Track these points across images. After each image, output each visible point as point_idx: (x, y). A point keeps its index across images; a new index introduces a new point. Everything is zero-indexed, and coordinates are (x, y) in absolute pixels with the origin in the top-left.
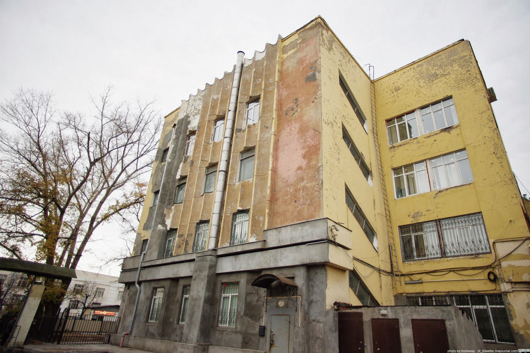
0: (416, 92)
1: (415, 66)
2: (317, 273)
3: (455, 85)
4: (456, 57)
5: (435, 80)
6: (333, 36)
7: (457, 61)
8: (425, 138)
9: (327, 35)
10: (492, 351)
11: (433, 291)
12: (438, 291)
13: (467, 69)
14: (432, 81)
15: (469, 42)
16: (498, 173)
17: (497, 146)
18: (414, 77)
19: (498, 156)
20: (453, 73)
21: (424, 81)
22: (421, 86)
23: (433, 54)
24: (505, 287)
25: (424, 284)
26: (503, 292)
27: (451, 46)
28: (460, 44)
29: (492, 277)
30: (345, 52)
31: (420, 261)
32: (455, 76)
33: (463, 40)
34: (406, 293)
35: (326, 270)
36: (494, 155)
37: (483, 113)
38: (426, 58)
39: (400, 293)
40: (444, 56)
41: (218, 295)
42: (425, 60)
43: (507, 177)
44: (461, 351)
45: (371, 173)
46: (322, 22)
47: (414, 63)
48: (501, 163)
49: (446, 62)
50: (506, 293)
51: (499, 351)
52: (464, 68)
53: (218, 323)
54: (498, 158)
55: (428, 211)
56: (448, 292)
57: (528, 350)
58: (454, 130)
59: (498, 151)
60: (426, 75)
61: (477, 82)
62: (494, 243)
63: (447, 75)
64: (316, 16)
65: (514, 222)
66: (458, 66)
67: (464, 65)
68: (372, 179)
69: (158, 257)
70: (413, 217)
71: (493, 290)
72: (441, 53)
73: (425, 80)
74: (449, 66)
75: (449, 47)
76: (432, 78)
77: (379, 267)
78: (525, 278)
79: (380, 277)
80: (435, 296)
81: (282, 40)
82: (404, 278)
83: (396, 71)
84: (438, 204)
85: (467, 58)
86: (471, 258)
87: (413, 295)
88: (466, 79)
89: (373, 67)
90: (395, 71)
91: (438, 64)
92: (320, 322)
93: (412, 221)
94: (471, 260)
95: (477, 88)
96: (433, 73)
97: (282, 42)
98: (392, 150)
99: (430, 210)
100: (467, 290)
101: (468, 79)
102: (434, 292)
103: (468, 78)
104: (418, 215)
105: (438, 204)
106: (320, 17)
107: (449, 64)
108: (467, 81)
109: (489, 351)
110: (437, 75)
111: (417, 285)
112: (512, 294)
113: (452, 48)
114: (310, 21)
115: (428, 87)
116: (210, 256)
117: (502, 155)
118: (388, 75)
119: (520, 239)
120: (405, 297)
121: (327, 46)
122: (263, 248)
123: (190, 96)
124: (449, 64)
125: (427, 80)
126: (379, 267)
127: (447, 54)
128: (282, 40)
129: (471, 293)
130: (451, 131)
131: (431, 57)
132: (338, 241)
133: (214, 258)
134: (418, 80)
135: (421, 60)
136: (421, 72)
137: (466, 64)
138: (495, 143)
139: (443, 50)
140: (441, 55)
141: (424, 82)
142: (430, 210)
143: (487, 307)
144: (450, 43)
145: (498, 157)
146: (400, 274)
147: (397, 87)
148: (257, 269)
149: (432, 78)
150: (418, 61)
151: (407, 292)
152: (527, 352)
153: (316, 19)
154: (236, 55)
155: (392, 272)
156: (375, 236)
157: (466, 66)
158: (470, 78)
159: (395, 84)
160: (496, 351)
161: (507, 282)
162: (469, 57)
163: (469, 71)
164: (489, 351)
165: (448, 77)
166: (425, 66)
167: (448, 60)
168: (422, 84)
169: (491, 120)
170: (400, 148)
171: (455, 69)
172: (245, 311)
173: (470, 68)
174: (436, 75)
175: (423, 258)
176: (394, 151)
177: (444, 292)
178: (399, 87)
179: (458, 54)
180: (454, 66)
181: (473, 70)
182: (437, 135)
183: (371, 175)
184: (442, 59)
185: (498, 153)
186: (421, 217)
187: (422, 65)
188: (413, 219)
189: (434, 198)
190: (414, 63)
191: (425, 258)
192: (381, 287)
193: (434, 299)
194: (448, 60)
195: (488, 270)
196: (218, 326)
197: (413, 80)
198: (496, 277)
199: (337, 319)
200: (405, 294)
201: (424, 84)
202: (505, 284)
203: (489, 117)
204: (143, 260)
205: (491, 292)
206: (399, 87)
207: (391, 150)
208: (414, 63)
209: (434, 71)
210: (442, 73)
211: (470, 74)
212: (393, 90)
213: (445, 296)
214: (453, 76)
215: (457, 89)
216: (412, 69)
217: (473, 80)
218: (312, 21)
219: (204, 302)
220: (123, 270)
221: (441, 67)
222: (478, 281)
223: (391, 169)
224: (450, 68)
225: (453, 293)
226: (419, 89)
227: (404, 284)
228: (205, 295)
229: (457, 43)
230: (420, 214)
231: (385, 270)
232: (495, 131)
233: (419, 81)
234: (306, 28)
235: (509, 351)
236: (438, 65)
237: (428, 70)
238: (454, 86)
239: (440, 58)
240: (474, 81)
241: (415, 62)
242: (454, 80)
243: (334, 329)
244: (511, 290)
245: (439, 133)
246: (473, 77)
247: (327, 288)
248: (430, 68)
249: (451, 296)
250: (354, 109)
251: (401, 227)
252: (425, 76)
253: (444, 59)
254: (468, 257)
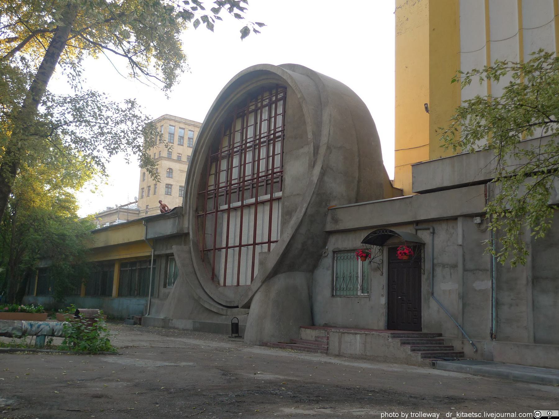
10: (476, 415)
44: (409, 415)
51: (492, 415)
57: (555, 414)
109: (470, 415)
138: (529, 130)
152: (552, 417)
160: (486, 415)
164: (470, 415)
235: (513, 415)
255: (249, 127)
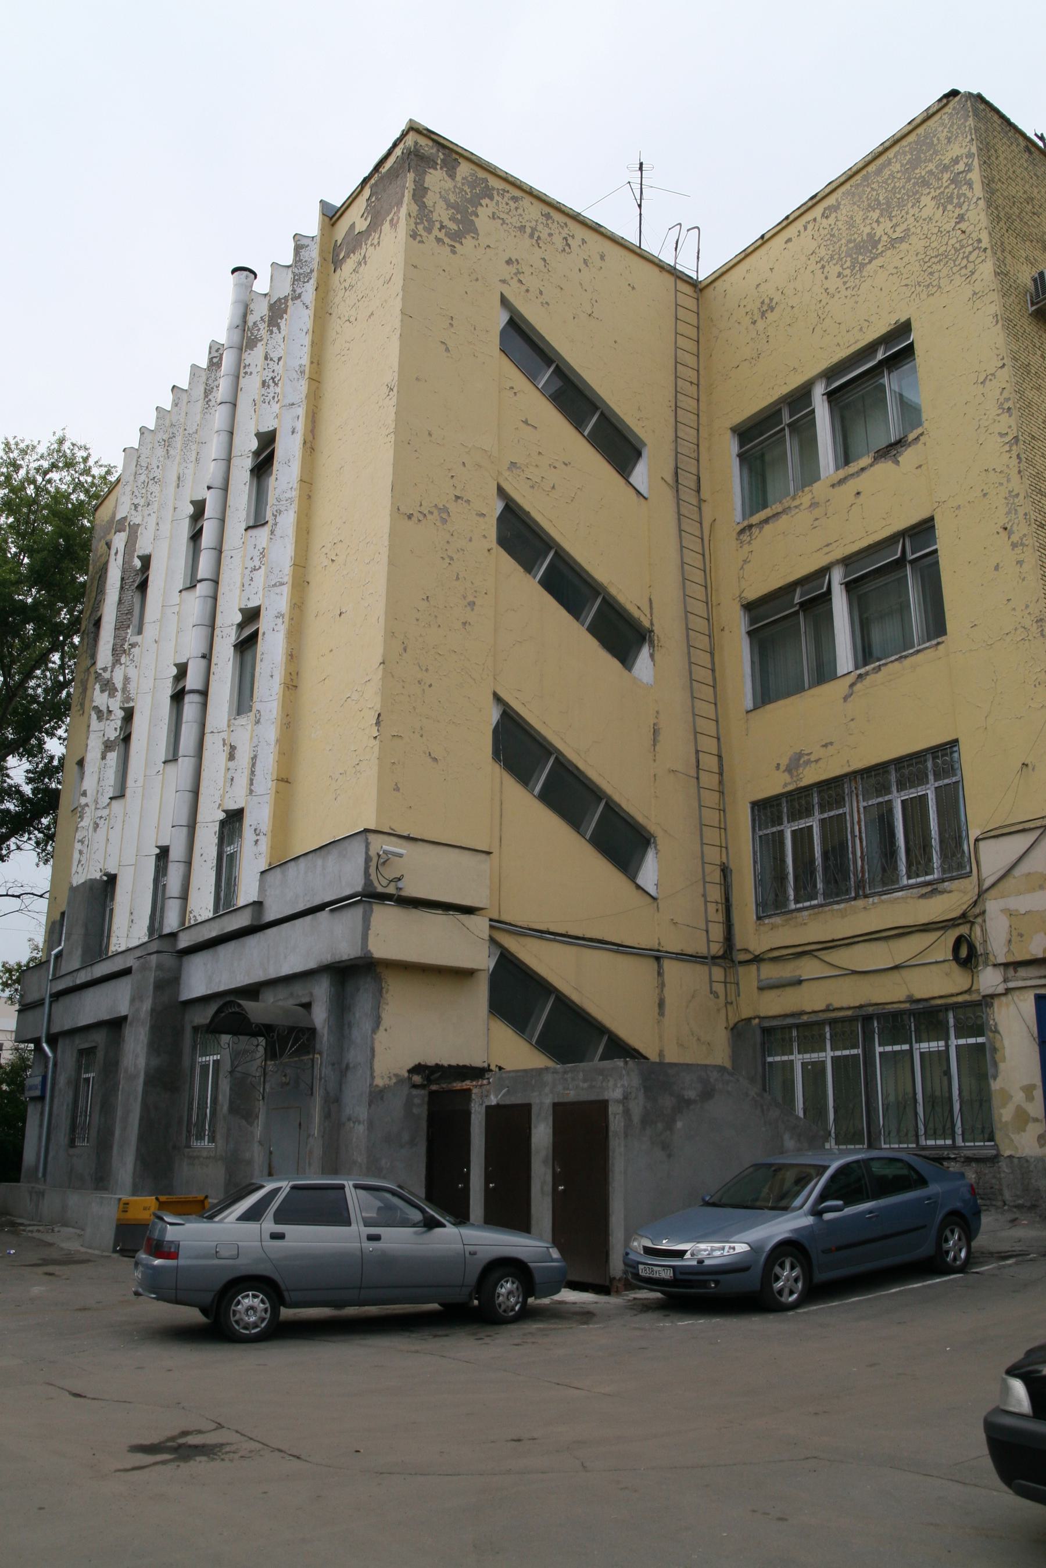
0: (816, 316)
1: (818, 211)
2: (358, 990)
3: (920, 279)
4: (931, 166)
5: (870, 262)
6: (482, 174)
7: (933, 181)
8: (833, 486)
9: (449, 184)
11: (823, 1007)
12: (836, 1005)
13: (958, 211)
14: (863, 266)
15: (980, 98)
16: (1009, 600)
17: (1016, 500)
18: (812, 258)
19: (1015, 538)
20: (918, 230)
21: (838, 268)
22: (831, 290)
23: (887, 144)
24: (989, 980)
25: (804, 984)
26: (984, 997)
27: (918, 121)
28: (946, 110)
29: (964, 953)
30: (548, 216)
31: (798, 914)
32: (923, 243)
33: (954, 93)
34: (759, 1017)
35: (378, 979)
36: (1004, 535)
37: (987, 382)
38: (851, 175)
39: (745, 1019)
40: (898, 166)
41: (186, 1062)
42: (847, 186)
43: (1029, 613)
45: (650, 636)
46: (423, 141)
47: (815, 200)
48: (1020, 563)
49: (904, 187)
50: (989, 1000)
52: (950, 207)
53: (188, 1138)
54: (1014, 546)
55: (825, 746)
56: (861, 1007)
58: (909, 450)
59: (1016, 521)
60: (846, 245)
61: (980, 260)
62: (977, 840)
63: (901, 240)
64: (403, 126)
65: (1033, 769)
66: (933, 203)
67: (950, 200)
68: (652, 656)
69: (83, 961)
70: (789, 770)
71: (965, 992)
72: (891, 154)
73: (842, 266)
74: (910, 204)
75: (914, 126)
76: (861, 258)
77: (659, 944)
78: (1035, 949)
79: (660, 974)
80: (833, 1022)
81: (331, 219)
82: (758, 970)
83: (767, 237)
84: (852, 720)
85: (961, 167)
86: (923, 896)
87: (774, 1023)
88: (953, 251)
89: (697, 230)
90: (762, 237)
91: (881, 198)
92: (359, 1123)
93: (785, 785)
94: (922, 902)
95: (978, 287)
96: (865, 237)
97: (333, 225)
98: (745, 537)
99: (831, 743)
100: (902, 999)
101: (956, 250)
102: (828, 1009)
103: (958, 246)
104: (801, 762)
105: (852, 720)
106: (413, 128)
107: (909, 196)
108: (954, 261)
110: (875, 244)
111: (789, 991)
112: (1004, 999)
113: (921, 130)
114: (390, 145)
115: (849, 292)
116: (155, 955)
117: (1025, 535)
118: (743, 255)
119: (1038, 823)
120: (758, 1032)
121: (442, 227)
122: (255, 923)
123: (142, 434)
124: (909, 196)
125: (848, 264)
126: (659, 944)
127: (909, 156)
128: (331, 219)
129: (914, 1006)
130: (901, 454)
131: (864, 172)
132: (412, 889)
133: (168, 960)
134: (823, 267)
135: (834, 185)
136: (833, 236)
137: (956, 191)
138: (1010, 492)
139: (896, 141)
140: (889, 162)
141: (839, 275)
142: (831, 743)
143: (947, 1046)
144: (916, 109)
145: (1015, 541)
146: (749, 957)
147: (767, 301)
148: (247, 985)
149: (861, 258)
150: (827, 191)
151: (762, 1015)
153: (404, 135)
154: (231, 279)
155: (725, 952)
156: (653, 846)
157: (955, 201)
158: (962, 247)
159: (762, 288)
161: (995, 965)
162: (966, 165)
163: (961, 218)
165: (904, 246)
166: (843, 211)
167: (909, 180)
168: (834, 283)
169: (1006, 406)
170: (767, 528)
171: (925, 213)
172: (231, 1103)
173: (965, 207)
174: (869, 247)
175: (807, 904)
176: (749, 543)
177: (849, 1008)
178: (771, 300)
179: (936, 153)
180: (922, 204)
181: (971, 215)
182: (864, 475)
183: (652, 644)
184: (892, 176)
185: (1015, 528)
186: (808, 768)
187: (835, 208)
188: (786, 777)
189: (845, 699)
190: (815, 201)
191: (815, 902)
192: (661, 1004)
193: (794, 1033)
194: (909, 180)
195: (952, 935)
196: (189, 1146)
197: (810, 269)
198: (972, 948)
199: (421, 1111)
200: (757, 1021)
201: (839, 282)
202: (989, 969)
203: (1001, 394)
204: (54, 974)
205: (960, 999)
206: (771, 300)
207: (741, 537)
208: (815, 201)
209: (867, 230)
210: (890, 232)
211: (964, 232)
212: (756, 311)
213: (851, 1020)
214: (917, 243)
215: (924, 296)
216: (810, 226)
217: (970, 253)
218: (395, 145)
219: (146, 1084)
220: (23, 1006)
221: (887, 210)
222: (933, 967)
223: (738, 607)
224: (911, 212)
225: (871, 1010)
226: (823, 303)
227: (756, 990)
228: (147, 1064)
229: (935, 109)
230: (806, 758)
231: (690, 951)
232: (1014, 447)
233: (826, 271)
234: (384, 170)
236: (879, 204)
237: (851, 224)
238: (919, 284)
239: (886, 173)
240: (972, 258)
241: (817, 198)
242: (920, 257)
243: (406, 1137)
244: (1001, 989)
245: (871, 465)
246: (970, 242)
247: (382, 1028)
248: (858, 219)
249: (867, 1019)
250: (577, 422)
251: (755, 805)
252: (844, 248)
253: (899, 175)
254: (915, 891)
255: (725, 969)
